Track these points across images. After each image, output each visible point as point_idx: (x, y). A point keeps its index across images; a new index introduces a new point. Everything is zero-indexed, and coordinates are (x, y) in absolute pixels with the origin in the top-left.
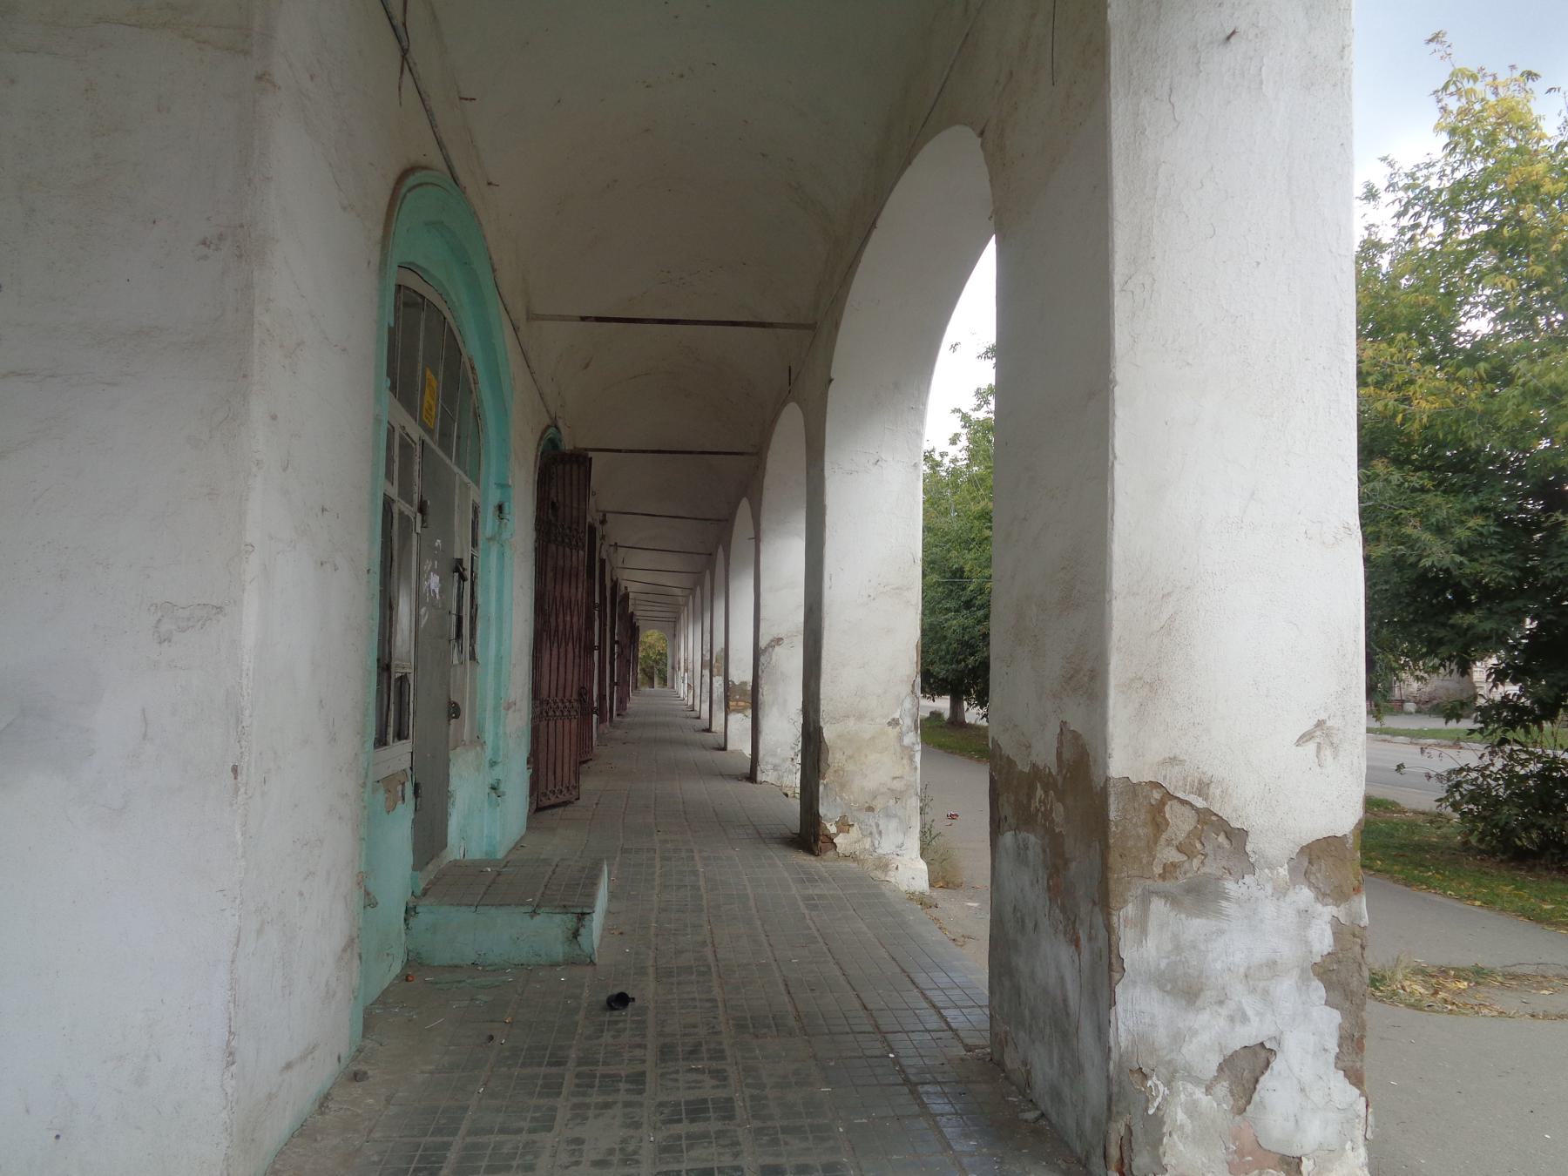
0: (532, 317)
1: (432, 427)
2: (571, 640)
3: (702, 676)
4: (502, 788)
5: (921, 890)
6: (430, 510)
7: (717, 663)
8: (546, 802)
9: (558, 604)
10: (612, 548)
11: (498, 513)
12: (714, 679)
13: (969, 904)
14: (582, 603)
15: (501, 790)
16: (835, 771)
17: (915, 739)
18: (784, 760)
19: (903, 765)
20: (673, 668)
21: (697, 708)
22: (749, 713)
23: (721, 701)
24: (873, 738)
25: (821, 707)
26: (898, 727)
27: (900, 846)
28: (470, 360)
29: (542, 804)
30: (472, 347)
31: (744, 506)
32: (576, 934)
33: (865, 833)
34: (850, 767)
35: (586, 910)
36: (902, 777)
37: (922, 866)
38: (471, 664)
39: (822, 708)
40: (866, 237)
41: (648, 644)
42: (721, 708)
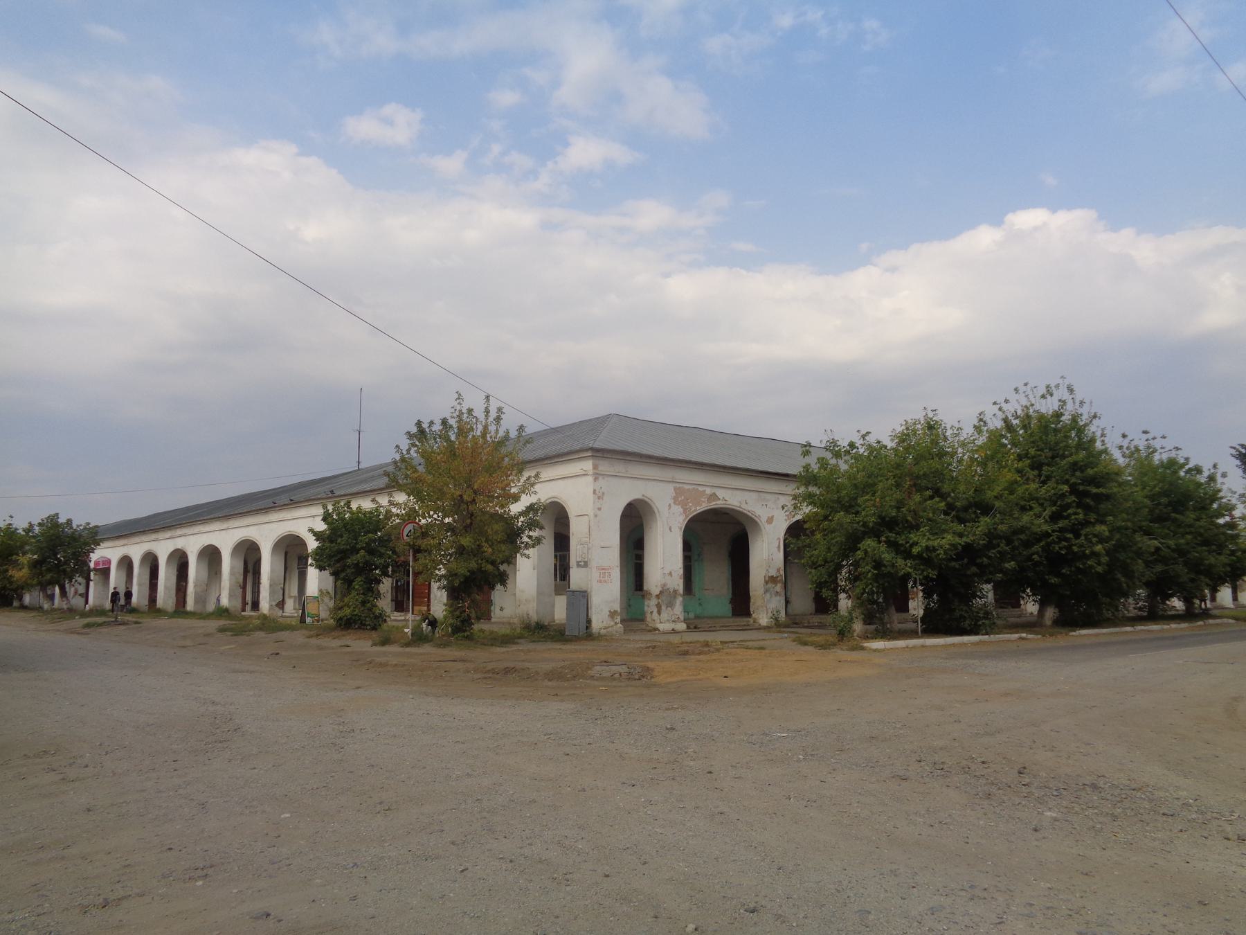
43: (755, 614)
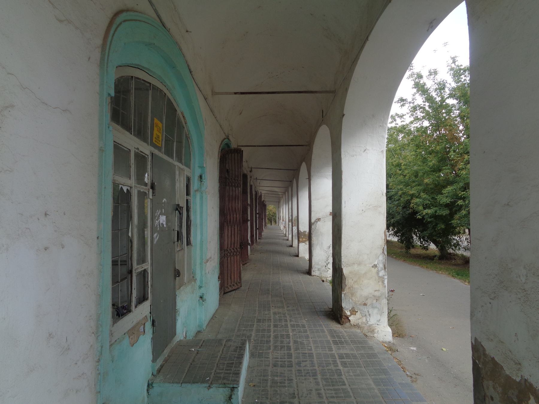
0: (214, 93)
1: (160, 146)
2: (236, 224)
3: (289, 225)
4: (204, 297)
5: (389, 340)
6: (157, 188)
7: (295, 221)
8: (227, 290)
9: (230, 211)
10: (255, 180)
11: (200, 179)
12: (293, 228)
13: (412, 348)
14: (240, 209)
15: (204, 298)
16: (349, 288)
17: (384, 273)
18: (322, 267)
19: (380, 285)
20: (278, 218)
21: (287, 235)
22: (307, 243)
23: (296, 236)
24: (365, 273)
25: (342, 259)
26: (377, 268)
27: (379, 321)
28: (182, 113)
29: (226, 291)
30: (182, 107)
31: (304, 166)
32: (230, 398)
33: (363, 315)
34: (356, 286)
35: (235, 386)
36: (379, 290)
37: (389, 330)
38: (187, 248)
39: (342, 260)
40: (362, 46)
41: (269, 210)
42: (296, 238)
43: (358, 315)
